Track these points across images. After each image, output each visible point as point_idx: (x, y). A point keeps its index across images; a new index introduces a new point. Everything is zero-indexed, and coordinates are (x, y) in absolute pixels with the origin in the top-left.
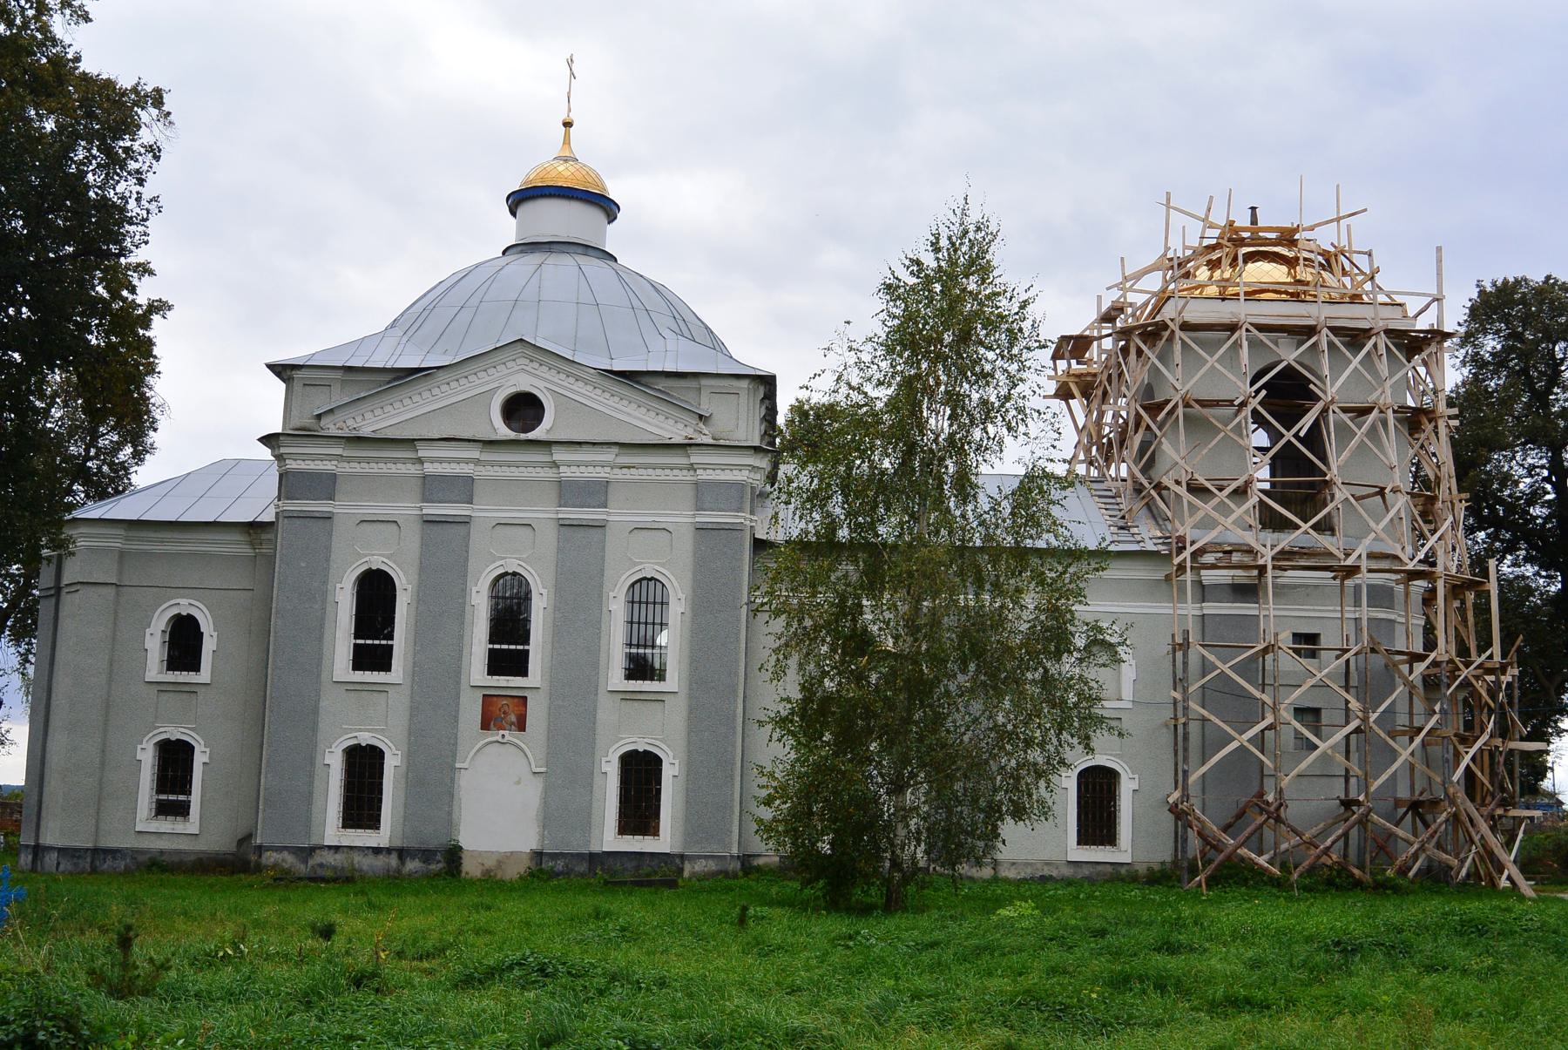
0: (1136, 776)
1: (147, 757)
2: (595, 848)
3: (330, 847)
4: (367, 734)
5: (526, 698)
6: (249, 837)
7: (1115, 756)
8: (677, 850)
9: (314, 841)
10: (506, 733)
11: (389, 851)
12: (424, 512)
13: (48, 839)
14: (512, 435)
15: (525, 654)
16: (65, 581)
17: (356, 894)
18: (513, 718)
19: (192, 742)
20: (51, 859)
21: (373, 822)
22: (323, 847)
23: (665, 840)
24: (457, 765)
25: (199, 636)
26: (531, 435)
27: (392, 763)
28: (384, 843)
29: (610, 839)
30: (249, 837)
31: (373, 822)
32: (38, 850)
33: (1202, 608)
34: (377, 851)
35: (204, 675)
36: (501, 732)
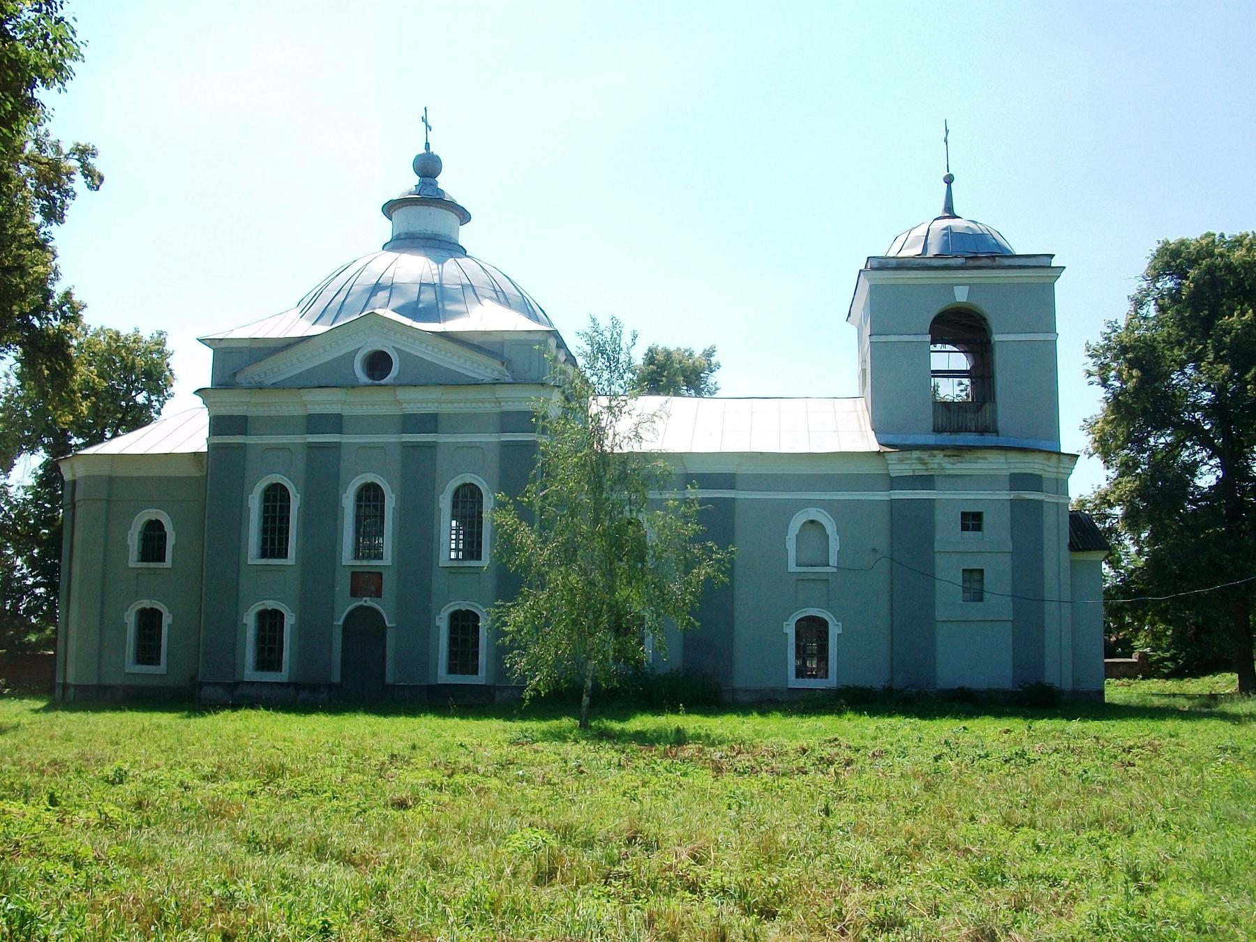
0: (840, 624)
1: (130, 619)
2: (432, 682)
3: (248, 682)
4: (270, 602)
5: (381, 574)
6: (194, 677)
7: (823, 608)
8: (490, 683)
9: (237, 678)
10: (368, 599)
11: (288, 684)
12: (308, 440)
13: (71, 680)
14: (370, 381)
15: (380, 546)
16: (76, 499)
17: (71, 180)
18: (373, 588)
19: (162, 610)
20: (71, 692)
21: (155, 660)
22: (243, 683)
23: (481, 678)
24: (335, 623)
25: (163, 538)
26: (382, 382)
27: (290, 620)
28: (285, 680)
29: (443, 676)
30: (194, 677)
31: (155, 660)
32: (65, 686)
33: (890, 495)
34: (281, 684)
35: (168, 564)
36: (365, 599)
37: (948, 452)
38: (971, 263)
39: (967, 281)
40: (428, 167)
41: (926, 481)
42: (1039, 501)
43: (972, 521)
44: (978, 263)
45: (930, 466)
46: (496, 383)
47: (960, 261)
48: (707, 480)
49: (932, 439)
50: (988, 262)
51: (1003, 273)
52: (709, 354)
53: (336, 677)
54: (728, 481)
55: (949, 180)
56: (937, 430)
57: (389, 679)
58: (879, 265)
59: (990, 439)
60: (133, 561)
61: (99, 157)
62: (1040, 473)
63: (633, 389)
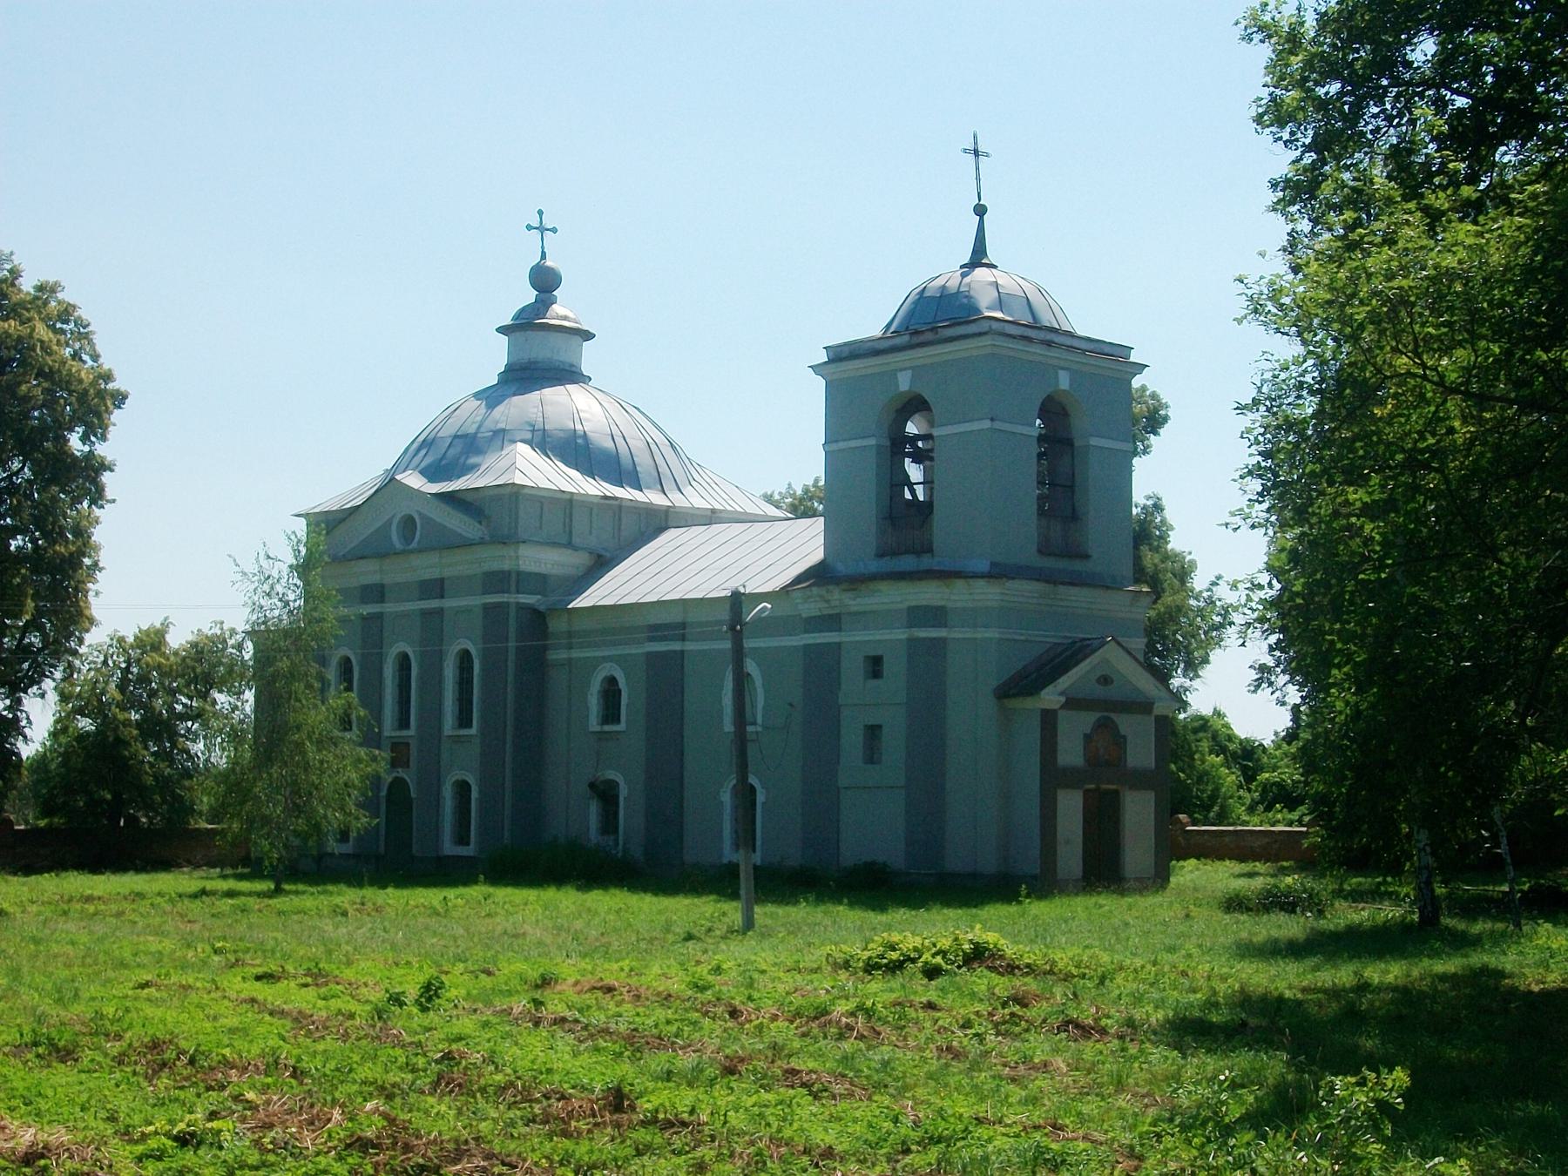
37: (844, 586)
38: (916, 340)
39: (908, 364)
40: (545, 281)
41: (832, 621)
42: (940, 639)
43: (875, 666)
44: (922, 338)
45: (833, 604)
46: (482, 542)
47: (906, 338)
48: (658, 631)
49: (874, 566)
50: (929, 336)
51: (940, 349)
52: (103, 568)
53: (382, 850)
54: (679, 630)
55: (980, 211)
56: (881, 555)
57: (415, 850)
58: (842, 355)
59: (926, 562)
60: (594, 724)
61: (116, 374)
62: (943, 603)
63: (1527, 405)
